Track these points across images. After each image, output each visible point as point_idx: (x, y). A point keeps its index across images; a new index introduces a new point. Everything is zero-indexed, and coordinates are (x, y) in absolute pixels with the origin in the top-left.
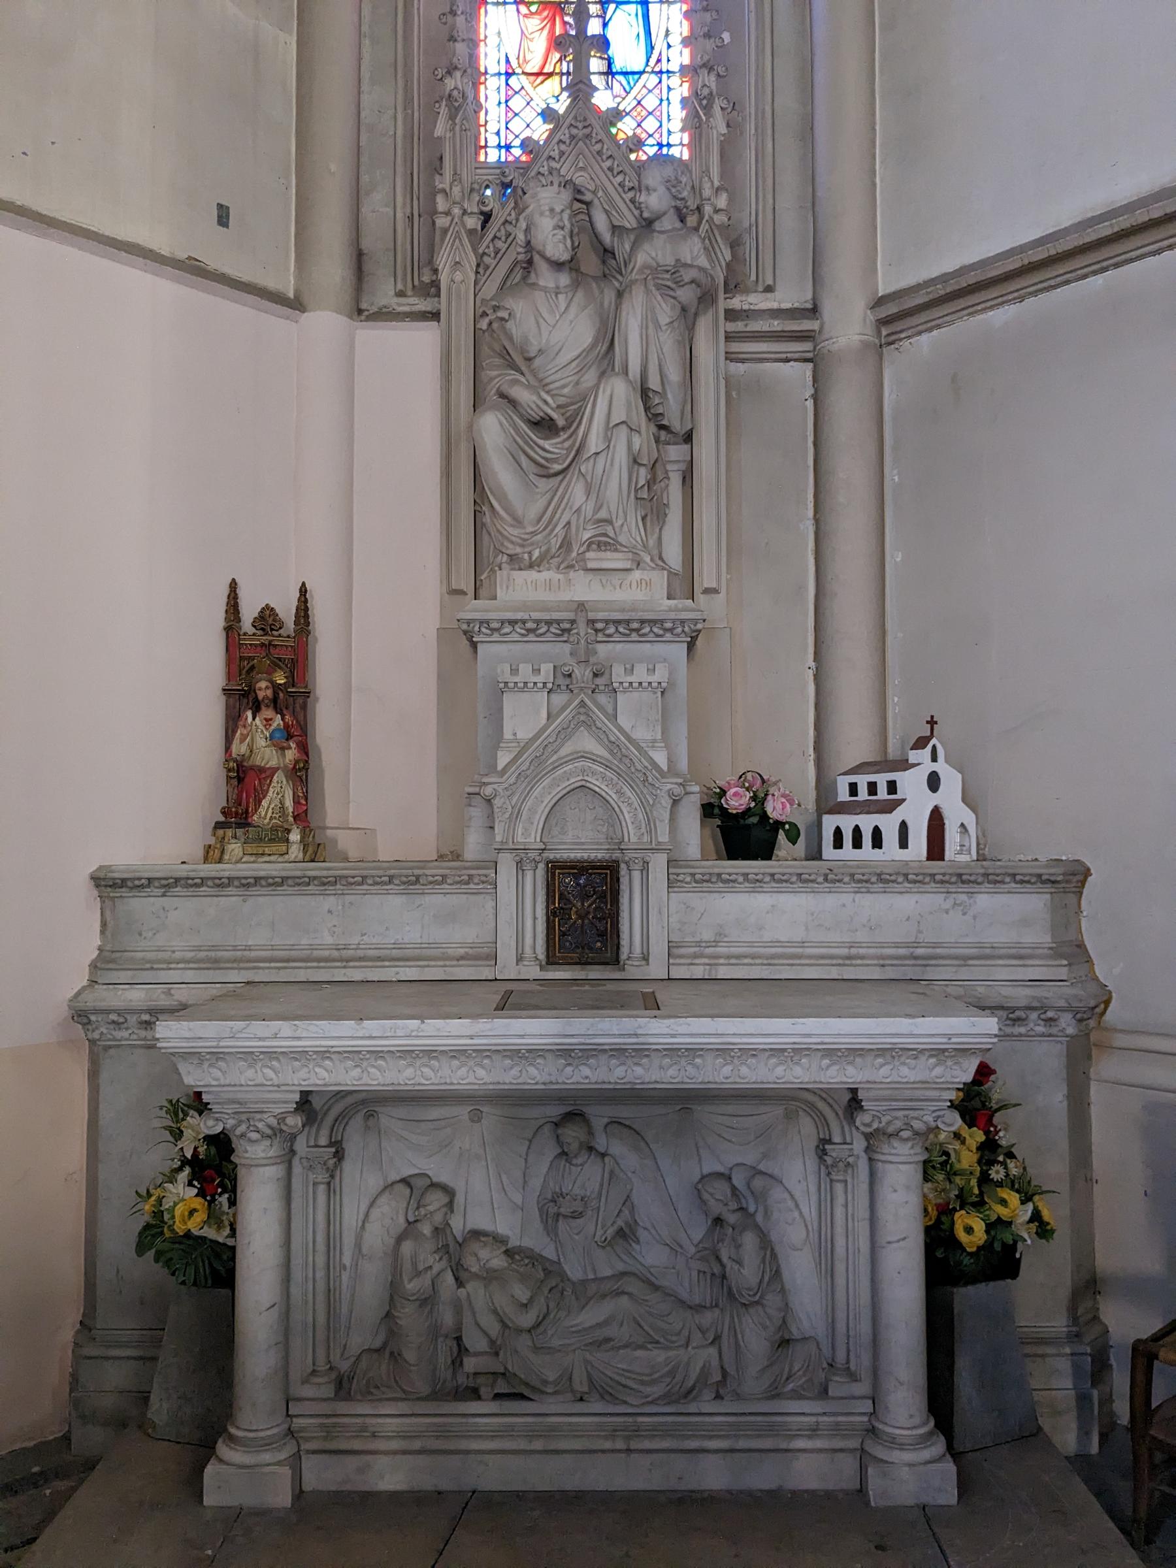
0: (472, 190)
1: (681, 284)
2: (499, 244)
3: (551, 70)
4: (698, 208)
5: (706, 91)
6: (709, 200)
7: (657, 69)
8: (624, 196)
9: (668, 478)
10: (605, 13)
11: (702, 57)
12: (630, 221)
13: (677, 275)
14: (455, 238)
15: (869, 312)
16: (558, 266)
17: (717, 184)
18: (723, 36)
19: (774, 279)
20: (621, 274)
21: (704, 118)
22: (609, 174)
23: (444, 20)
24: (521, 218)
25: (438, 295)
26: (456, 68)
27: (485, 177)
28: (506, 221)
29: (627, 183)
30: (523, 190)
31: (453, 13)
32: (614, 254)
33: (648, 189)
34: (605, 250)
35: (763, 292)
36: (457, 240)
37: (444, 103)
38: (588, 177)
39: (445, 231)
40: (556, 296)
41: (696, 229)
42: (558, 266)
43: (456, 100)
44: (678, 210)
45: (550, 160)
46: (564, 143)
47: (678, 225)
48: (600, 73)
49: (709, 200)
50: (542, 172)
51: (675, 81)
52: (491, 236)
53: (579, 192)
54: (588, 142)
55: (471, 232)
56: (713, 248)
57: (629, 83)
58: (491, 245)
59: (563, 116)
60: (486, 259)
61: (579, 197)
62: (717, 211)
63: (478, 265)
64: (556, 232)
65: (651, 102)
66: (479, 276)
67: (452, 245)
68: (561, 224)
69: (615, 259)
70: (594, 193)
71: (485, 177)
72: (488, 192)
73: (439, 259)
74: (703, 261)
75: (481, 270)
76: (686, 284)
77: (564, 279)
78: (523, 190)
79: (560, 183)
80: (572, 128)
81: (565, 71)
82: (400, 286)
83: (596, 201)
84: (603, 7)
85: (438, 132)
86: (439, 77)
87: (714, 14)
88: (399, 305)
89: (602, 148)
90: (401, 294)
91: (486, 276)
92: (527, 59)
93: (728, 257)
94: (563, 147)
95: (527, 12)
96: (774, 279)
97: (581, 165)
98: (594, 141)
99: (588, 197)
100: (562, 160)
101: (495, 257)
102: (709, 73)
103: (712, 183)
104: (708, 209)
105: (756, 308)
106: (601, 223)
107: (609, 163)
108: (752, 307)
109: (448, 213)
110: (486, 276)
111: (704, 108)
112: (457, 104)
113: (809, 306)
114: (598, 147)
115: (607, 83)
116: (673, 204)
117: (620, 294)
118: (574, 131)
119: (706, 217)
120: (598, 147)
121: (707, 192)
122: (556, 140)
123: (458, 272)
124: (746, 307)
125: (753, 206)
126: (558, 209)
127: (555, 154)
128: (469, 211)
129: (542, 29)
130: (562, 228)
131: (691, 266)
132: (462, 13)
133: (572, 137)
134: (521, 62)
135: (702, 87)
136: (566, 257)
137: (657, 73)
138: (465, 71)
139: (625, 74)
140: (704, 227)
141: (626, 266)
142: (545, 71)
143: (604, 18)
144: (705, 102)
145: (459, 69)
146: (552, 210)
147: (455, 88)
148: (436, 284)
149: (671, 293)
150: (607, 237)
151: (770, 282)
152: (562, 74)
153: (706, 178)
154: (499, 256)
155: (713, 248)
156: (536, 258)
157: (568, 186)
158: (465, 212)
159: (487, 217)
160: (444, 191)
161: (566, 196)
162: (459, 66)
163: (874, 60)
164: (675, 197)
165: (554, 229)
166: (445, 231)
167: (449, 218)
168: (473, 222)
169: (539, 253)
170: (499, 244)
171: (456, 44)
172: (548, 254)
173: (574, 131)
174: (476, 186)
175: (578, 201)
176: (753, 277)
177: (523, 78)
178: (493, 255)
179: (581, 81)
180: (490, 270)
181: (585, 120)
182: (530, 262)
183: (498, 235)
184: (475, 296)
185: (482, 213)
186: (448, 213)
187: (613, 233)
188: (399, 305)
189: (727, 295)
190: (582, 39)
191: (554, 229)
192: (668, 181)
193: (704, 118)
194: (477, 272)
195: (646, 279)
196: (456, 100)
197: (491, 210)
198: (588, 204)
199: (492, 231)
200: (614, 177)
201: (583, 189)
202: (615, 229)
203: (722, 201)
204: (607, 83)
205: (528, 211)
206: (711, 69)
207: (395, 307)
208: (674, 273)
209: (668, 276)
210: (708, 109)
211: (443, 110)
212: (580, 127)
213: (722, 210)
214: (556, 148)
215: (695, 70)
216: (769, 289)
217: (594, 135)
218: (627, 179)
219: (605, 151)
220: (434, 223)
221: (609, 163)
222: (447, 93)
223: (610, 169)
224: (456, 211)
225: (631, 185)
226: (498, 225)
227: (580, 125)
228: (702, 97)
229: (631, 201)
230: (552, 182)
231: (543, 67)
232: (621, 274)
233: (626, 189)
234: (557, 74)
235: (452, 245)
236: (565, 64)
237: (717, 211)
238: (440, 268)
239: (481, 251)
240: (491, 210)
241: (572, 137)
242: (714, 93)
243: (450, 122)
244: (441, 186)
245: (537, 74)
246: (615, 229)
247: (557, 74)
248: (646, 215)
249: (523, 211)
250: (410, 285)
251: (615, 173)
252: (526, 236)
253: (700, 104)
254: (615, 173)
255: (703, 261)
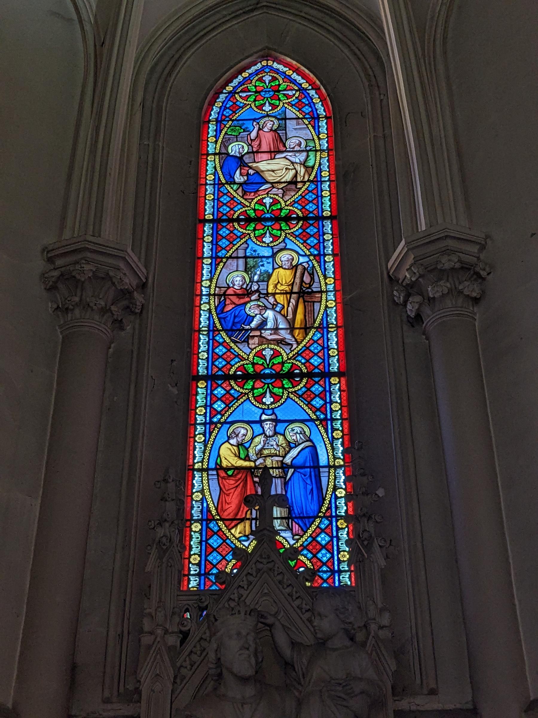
0: (174, 613)
1: (353, 695)
2: (194, 657)
3: (244, 516)
4: (365, 626)
5: (366, 535)
6: (374, 619)
7: (328, 514)
8: (302, 616)
9: (361, 631)
10: (286, 475)
11: (361, 509)
12: (307, 639)
13: (349, 687)
14: (157, 654)
15: (523, 714)
16: (244, 680)
17: (380, 605)
18: (377, 492)
19: (437, 683)
20: (300, 684)
21: (366, 555)
22: (290, 599)
23: (158, 486)
24: (213, 639)
25: (139, 701)
26: (166, 520)
27: (185, 602)
28: (201, 638)
29: (304, 606)
30: (215, 618)
31: (166, 481)
32: (293, 666)
33: (320, 614)
34: (286, 663)
35: (429, 694)
36: (158, 656)
37: (155, 546)
38: (272, 601)
39: (149, 647)
40: (242, 706)
41: (364, 644)
42: (244, 680)
43: (164, 545)
44: (346, 631)
45: (240, 588)
46: (251, 575)
47: (348, 643)
48: (281, 518)
49: (374, 619)
50: (233, 598)
51: (341, 523)
52: (189, 650)
53: (262, 616)
54: (272, 574)
55: (170, 649)
56: (379, 659)
57: (305, 524)
58: (187, 659)
59: (250, 554)
60: (184, 671)
61: (262, 620)
62: (381, 628)
63: (175, 677)
64: (241, 652)
65: (323, 539)
66: (175, 685)
67: (155, 659)
68: (247, 646)
69: (294, 670)
70: (275, 615)
71: (185, 602)
72: (188, 615)
73: (141, 673)
74: (371, 673)
75: (178, 681)
76: (356, 696)
77: (250, 691)
78: (215, 618)
79: (246, 611)
80: (258, 564)
81: (254, 516)
82: (107, 694)
83: (277, 623)
84: (284, 472)
85: (148, 569)
86: (152, 527)
87: (370, 478)
88: (104, 710)
89: (283, 578)
90: (107, 701)
91: (183, 685)
92: (224, 508)
93: (394, 667)
94: (251, 578)
95: (225, 475)
96: (437, 683)
97: (266, 591)
98: (276, 573)
99: (270, 620)
100: (250, 588)
101: (201, 654)
102: (368, 520)
103: (376, 605)
104: (373, 627)
105: (422, 709)
106: (282, 640)
107: (289, 590)
108: (419, 708)
109: (151, 633)
110: (183, 685)
111: (365, 547)
112: (165, 547)
113: (470, 706)
114: (279, 577)
115: (288, 525)
116: (342, 626)
117: (300, 703)
118: (260, 566)
119: (372, 634)
120: (279, 577)
121: (372, 613)
122: (245, 572)
123: (158, 683)
124: (414, 708)
125: (413, 621)
126: (244, 633)
127: (245, 584)
128: (170, 631)
129: (237, 487)
130: (248, 649)
131: (361, 679)
132: (173, 481)
133: (258, 570)
134: (219, 511)
135: (363, 531)
136: (250, 672)
137: (327, 518)
138: (173, 522)
139: (302, 518)
140: (371, 641)
141: (304, 678)
142: (238, 517)
143: (285, 478)
144: (366, 543)
145: (168, 522)
146: (239, 634)
147: (165, 536)
148: (138, 691)
149: (344, 703)
150: (287, 652)
151: (433, 685)
152: (251, 519)
153: (371, 602)
154: (195, 666)
155: (379, 659)
156: (225, 672)
157: (252, 614)
158: (166, 632)
159: (185, 636)
160: (150, 614)
161: (251, 621)
162: (168, 519)
163: (500, 509)
164: (344, 622)
165: (241, 649)
166: (149, 647)
167: (153, 637)
168: (173, 640)
169: (227, 669)
170: (194, 657)
171: (167, 503)
172: (235, 671)
173: (260, 566)
174: (176, 610)
175: (262, 623)
176: (418, 681)
177: (220, 523)
178: (189, 667)
179: (264, 529)
180: (187, 679)
181: (269, 557)
182: (220, 675)
183: (194, 650)
184: (171, 703)
185: (181, 632)
186: (151, 633)
187: (293, 648)
188: (104, 710)
189: (396, 698)
190: (265, 498)
191: (241, 649)
192: (336, 610)
193: (366, 555)
194: (175, 682)
195: (321, 691)
196: (164, 545)
197: (189, 630)
198: (271, 626)
199: (188, 648)
200: (293, 601)
201: (265, 615)
202: (294, 644)
203: (385, 620)
204: (288, 525)
205: (219, 634)
206: (369, 518)
207: (101, 712)
208: (346, 685)
209: (340, 688)
210: (368, 548)
211: (154, 552)
212: (265, 563)
213: (386, 627)
214: (245, 579)
215: (357, 519)
216: (433, 692)
217: (276, 569)
218: (304, 602)
219: (285, 580)
220: (140, 640)
221: (289, 590)
222: (157, 539)
223: (290, 595)
224: (159, 631)
225: (308, 607)
226: (184, 656)
227: (265, 561)
228: (363, 539)
229: (308, 620)
230: (239, 611)
231: (237, 514)
232: (300, 684)
233: (304, 611)
234: (248, 519)
235: (155, 659)
236: (254, 512)
237: (381, 628)
238: (142, 680)
239: (178, 664)
240: (189, 630)
241: (258, 570)
242: (373, 535)
243: (159, 560)
244: (148, 611)
245: (232, 520)
246: (294, 644)
247: (248, 519)
248: (319, 636)
249: (215, 634)
250: (115, 693)
251: (294, 598)
252: (217, 654)
253: (362, 544)
254: (294, 598)
255: (371, 673)
